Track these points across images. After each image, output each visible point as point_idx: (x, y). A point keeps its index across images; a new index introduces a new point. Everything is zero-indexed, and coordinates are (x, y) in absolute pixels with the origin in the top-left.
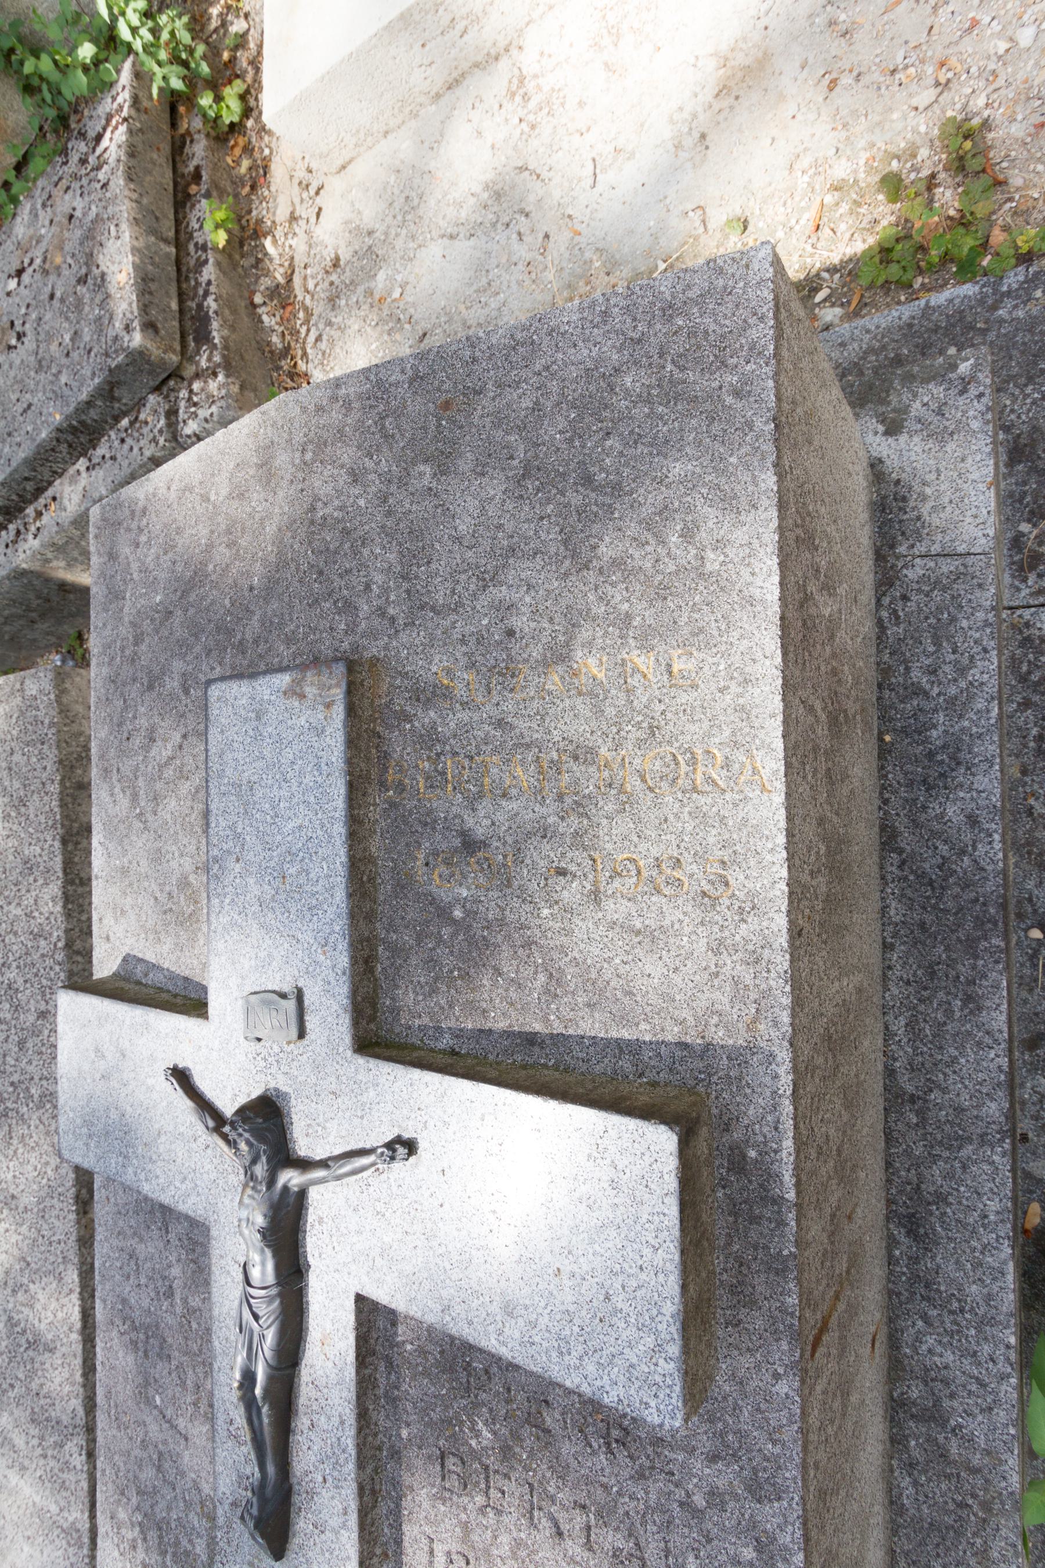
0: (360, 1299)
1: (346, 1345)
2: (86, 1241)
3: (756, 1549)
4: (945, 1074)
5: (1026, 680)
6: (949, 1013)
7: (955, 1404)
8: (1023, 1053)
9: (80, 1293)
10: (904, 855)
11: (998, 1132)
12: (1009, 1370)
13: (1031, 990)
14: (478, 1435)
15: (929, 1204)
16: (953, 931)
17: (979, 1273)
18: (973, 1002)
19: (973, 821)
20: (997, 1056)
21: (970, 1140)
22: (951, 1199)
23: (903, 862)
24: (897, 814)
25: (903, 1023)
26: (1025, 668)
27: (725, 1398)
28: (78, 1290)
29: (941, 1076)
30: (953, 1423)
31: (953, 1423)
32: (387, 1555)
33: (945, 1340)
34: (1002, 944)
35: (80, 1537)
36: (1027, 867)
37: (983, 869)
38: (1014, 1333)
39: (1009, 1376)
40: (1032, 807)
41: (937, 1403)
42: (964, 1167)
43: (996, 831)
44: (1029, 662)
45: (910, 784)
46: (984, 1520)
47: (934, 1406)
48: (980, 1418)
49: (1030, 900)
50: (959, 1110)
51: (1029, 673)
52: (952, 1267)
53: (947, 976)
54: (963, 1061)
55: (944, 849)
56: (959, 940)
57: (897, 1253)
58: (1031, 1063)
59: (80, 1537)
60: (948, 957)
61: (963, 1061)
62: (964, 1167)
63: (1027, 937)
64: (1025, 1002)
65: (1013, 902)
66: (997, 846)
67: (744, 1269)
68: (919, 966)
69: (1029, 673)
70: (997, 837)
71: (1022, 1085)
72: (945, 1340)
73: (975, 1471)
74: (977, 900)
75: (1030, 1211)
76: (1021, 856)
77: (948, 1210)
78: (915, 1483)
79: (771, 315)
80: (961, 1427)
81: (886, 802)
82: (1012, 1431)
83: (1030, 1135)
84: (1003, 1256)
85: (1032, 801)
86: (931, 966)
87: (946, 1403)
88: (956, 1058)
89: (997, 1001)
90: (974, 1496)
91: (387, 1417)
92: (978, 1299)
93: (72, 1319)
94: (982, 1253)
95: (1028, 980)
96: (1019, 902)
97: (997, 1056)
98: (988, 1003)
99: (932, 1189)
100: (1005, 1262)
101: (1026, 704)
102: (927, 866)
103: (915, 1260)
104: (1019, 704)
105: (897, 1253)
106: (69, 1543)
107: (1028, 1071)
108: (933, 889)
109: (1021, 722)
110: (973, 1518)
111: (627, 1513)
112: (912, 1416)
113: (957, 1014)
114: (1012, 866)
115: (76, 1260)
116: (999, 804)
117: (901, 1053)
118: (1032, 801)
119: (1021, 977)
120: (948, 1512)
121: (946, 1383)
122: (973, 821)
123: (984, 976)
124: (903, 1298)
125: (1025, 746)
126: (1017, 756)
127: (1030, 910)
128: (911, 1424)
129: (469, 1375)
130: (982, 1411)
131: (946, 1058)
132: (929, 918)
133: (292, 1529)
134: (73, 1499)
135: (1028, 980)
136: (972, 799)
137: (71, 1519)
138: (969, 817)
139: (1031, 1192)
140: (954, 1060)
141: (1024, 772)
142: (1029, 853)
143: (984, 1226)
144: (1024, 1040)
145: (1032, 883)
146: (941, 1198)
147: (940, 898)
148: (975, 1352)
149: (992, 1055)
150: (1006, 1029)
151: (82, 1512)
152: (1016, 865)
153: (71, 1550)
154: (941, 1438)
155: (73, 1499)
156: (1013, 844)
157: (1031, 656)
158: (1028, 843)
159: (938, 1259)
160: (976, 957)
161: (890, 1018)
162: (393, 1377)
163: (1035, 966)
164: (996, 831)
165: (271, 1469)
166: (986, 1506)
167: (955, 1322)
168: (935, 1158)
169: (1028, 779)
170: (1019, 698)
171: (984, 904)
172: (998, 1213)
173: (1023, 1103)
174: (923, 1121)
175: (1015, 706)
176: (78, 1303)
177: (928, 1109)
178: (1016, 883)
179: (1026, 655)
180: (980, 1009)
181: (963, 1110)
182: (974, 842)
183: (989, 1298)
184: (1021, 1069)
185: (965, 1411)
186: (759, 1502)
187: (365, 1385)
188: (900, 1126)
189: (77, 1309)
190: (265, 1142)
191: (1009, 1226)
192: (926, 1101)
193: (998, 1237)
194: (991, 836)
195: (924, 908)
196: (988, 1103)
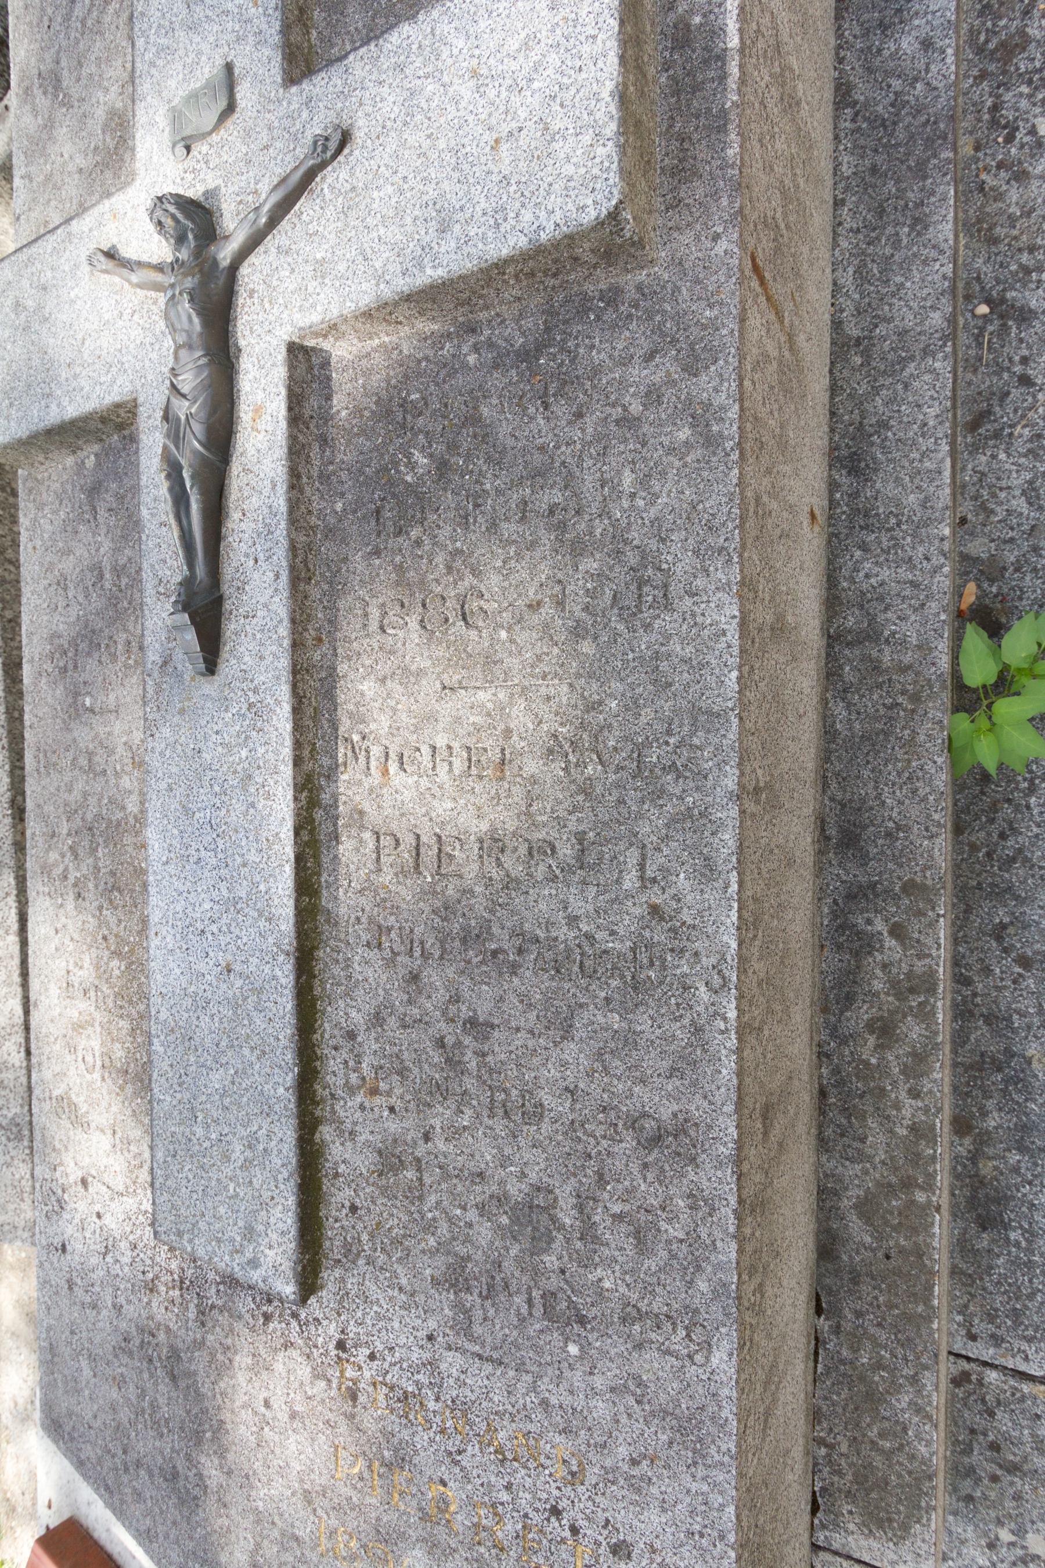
0: (291, 79)
1: (277, 407)
2: (20, 847)
3: (693, 426)
4: (890, 305)
5: (983, 51)
6: (896, 244)
7: (889, 615)
8: (965, 437)
9: (17, 896)
10: (858, 107)
11: (941, 339)
12: (942, 560)
13: (975, 371)
14: (412, 466)
15: (871, 435)
16: (902, 162)
17: (916, 481)
18: (920, 223)
19: (927, 44)
20: (942, 265)
21: (912, 358)
22: (892, 422)
23: (856, 114)
24: (853, 69)
25: (851, 273)
26: (982, 38)
27: (663, 287)
28: (15, 892)
29: (887, 308)
30: (886, 633)
31: (886, 633)
32: (320, 640)
33: (882, 559)
34: (951, 155)
35: (19, 1131)
36: (977, 246)
37: (936, 89)
38: (949, 525)
39: (942, 566)
40: (984, 182)
41: (872, 620)
42: (906, 386)
43: (949, 46)
44: (987, 30)
45: (866, 34)
46: (913, 711)
47: (869, 625)
48: (913, 618)
49: (978, 278)
50: (902, 333)
51: (987, 41)
52: (891, 485)
53: (896, 208)
54: (908, 284)
55: (896, 84)
56: (909, 168)
57: (838, 495)
58: (973, 444)
59: (19, 1131)
60: (898, 190)
61: (908, 284)
62: (906, 386)
63: (974, 316)
64: (969, 383)
65: (960, 285)
66: (950, 59)
67: (686, 145)
68: (869, 211)
69: (987, 41)
70: (950, 51)
71: (964, 469)
72: (882, 559)
73: (904, 669)
74: (928, 121)
75: (966, 591)
76: (972, 236)
77: (890, 434)
78: (849, 705)
79: (730, 1108)
80: (894, 633)
81: (841, 60)
82: (943, 617)
83: (969, 516)
84: (940, 455)
85: (984, 176)
86: (881, 205)
87: (881, 618)
88: (902, 284)
89: (944, 212)
90: (904, 692)
91: (322, 498)
92: (915, 507)
93: (9, 922)
94: (920, 461)
95: (972, 361)
96: (967, 283)
97: (942, 265)
98: (936, 218)
99: (874, 421)
100: (942, 460)
101: (983, 75)
102: (880, 108)
103: (855, 495)
104: (975, 78)
105: (838, 495)
106: (9, 1139)
107: (970, 453)
108: (885, 127)
109: (976, 98)
110: (902, 713)
111: (563, 463)
112: (848, 644)
113: (905, 241)
114: (962, 248)
115: (12, 864)
116: (953, 18)
117: (849, 303)
118: (984, 176)
119: (967, 360)
120: (877, 719)
121: (881, 599)
122: (927, 44)
123: (933, 193)
124: (842, 536)
125: (979, 120)
126: (971, 133)
127: (978, 288)
128: (847, 652)
129: (405, 411)
130: (915, 610)
131: (893, 288)
132: (879, 159)
133: (223, 640)
134: (12, 1096)
135: (972, 361)
136: (927, 22)
137: (10, 1115)
138: (922, 43)
139: (967, 573)
140: (901, 286)
141: (977, 149)
142: (979, 231)
143: (923, 435)
144: (967, 423)
145: (980, 261)
146: (884, 425)
147: (891, 135)
148: (910, 558)
149: (937, 267)
150: (951, 237)
151: (22, 1106)
152: (966, 246)
153: (11, 1145)
154: (874, 653)
155: (12, 1096)
156: (964, 225)
157: (989, 24)
158: (979, 221)
159: (878, 485)
160: (925, 178)
161: (839, 273)
162: (327, 453)
163: (980, 345)
164: (949, 46)
165: (200, 570)
166: (916, 698)
167: (892, 538)
168: (876, 390)
169: (980, 155)
170: (975, 72)
171: (935, 123)
172: (937, 416)
173: (964, 486)
174: (866, 363)
175: (971, 81)
176: (15, 905)
177: (874, 345)
178: (965, 265)
179: (984, 23)
180: (926, 228)
181: (907, 332)
182: (928, 65)
183: (924, 504)
184: (962, 453)
185: (899, 618)
186: (695, 375)
187: (296, 452)
188: (846, 373)
189: (14, 911)
190: (193, 221)
191: (947, 424)
192: (871, 338)
193: (936, 439)
194: (944, 52)
195: (876, 151)
196: (932, 315)
